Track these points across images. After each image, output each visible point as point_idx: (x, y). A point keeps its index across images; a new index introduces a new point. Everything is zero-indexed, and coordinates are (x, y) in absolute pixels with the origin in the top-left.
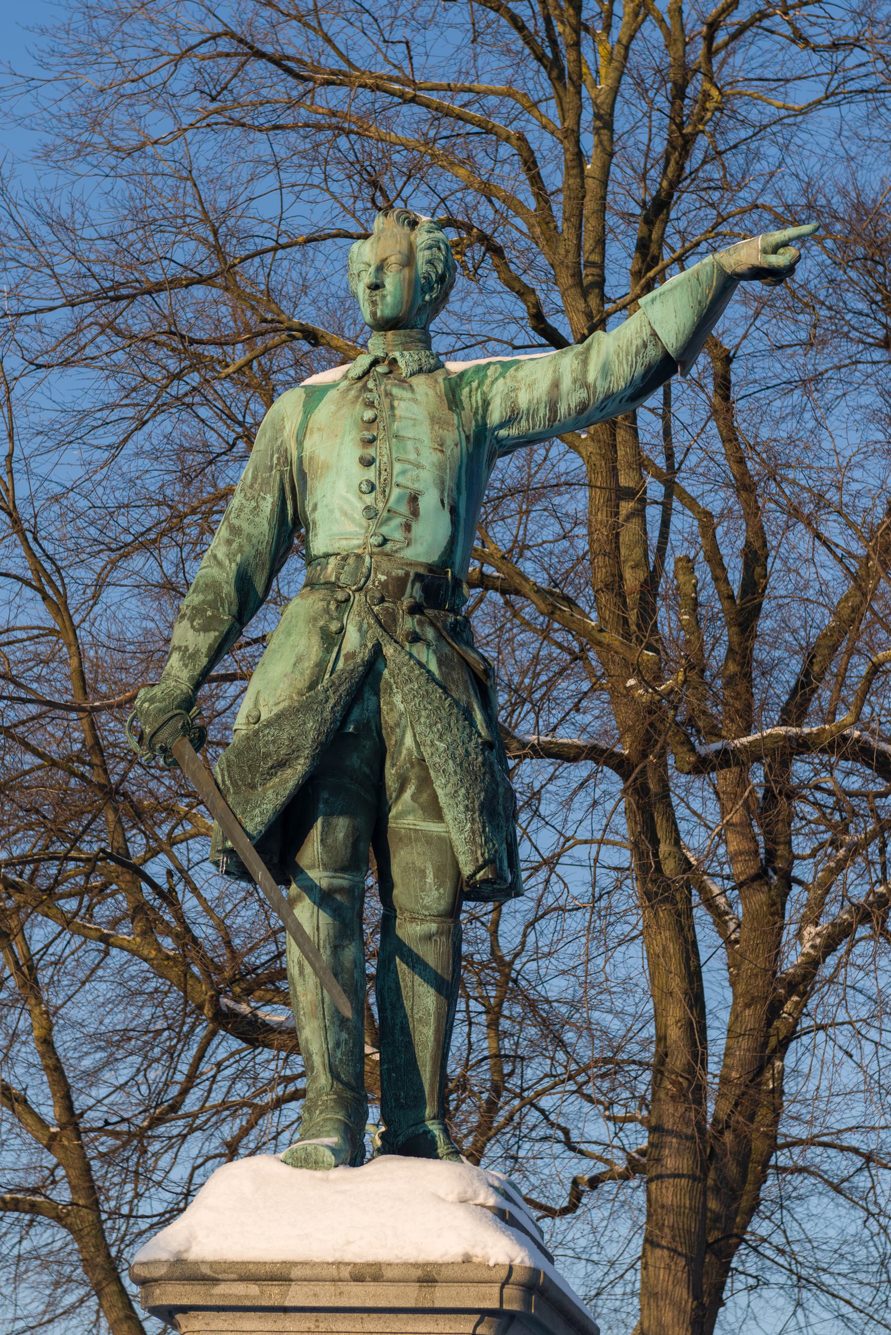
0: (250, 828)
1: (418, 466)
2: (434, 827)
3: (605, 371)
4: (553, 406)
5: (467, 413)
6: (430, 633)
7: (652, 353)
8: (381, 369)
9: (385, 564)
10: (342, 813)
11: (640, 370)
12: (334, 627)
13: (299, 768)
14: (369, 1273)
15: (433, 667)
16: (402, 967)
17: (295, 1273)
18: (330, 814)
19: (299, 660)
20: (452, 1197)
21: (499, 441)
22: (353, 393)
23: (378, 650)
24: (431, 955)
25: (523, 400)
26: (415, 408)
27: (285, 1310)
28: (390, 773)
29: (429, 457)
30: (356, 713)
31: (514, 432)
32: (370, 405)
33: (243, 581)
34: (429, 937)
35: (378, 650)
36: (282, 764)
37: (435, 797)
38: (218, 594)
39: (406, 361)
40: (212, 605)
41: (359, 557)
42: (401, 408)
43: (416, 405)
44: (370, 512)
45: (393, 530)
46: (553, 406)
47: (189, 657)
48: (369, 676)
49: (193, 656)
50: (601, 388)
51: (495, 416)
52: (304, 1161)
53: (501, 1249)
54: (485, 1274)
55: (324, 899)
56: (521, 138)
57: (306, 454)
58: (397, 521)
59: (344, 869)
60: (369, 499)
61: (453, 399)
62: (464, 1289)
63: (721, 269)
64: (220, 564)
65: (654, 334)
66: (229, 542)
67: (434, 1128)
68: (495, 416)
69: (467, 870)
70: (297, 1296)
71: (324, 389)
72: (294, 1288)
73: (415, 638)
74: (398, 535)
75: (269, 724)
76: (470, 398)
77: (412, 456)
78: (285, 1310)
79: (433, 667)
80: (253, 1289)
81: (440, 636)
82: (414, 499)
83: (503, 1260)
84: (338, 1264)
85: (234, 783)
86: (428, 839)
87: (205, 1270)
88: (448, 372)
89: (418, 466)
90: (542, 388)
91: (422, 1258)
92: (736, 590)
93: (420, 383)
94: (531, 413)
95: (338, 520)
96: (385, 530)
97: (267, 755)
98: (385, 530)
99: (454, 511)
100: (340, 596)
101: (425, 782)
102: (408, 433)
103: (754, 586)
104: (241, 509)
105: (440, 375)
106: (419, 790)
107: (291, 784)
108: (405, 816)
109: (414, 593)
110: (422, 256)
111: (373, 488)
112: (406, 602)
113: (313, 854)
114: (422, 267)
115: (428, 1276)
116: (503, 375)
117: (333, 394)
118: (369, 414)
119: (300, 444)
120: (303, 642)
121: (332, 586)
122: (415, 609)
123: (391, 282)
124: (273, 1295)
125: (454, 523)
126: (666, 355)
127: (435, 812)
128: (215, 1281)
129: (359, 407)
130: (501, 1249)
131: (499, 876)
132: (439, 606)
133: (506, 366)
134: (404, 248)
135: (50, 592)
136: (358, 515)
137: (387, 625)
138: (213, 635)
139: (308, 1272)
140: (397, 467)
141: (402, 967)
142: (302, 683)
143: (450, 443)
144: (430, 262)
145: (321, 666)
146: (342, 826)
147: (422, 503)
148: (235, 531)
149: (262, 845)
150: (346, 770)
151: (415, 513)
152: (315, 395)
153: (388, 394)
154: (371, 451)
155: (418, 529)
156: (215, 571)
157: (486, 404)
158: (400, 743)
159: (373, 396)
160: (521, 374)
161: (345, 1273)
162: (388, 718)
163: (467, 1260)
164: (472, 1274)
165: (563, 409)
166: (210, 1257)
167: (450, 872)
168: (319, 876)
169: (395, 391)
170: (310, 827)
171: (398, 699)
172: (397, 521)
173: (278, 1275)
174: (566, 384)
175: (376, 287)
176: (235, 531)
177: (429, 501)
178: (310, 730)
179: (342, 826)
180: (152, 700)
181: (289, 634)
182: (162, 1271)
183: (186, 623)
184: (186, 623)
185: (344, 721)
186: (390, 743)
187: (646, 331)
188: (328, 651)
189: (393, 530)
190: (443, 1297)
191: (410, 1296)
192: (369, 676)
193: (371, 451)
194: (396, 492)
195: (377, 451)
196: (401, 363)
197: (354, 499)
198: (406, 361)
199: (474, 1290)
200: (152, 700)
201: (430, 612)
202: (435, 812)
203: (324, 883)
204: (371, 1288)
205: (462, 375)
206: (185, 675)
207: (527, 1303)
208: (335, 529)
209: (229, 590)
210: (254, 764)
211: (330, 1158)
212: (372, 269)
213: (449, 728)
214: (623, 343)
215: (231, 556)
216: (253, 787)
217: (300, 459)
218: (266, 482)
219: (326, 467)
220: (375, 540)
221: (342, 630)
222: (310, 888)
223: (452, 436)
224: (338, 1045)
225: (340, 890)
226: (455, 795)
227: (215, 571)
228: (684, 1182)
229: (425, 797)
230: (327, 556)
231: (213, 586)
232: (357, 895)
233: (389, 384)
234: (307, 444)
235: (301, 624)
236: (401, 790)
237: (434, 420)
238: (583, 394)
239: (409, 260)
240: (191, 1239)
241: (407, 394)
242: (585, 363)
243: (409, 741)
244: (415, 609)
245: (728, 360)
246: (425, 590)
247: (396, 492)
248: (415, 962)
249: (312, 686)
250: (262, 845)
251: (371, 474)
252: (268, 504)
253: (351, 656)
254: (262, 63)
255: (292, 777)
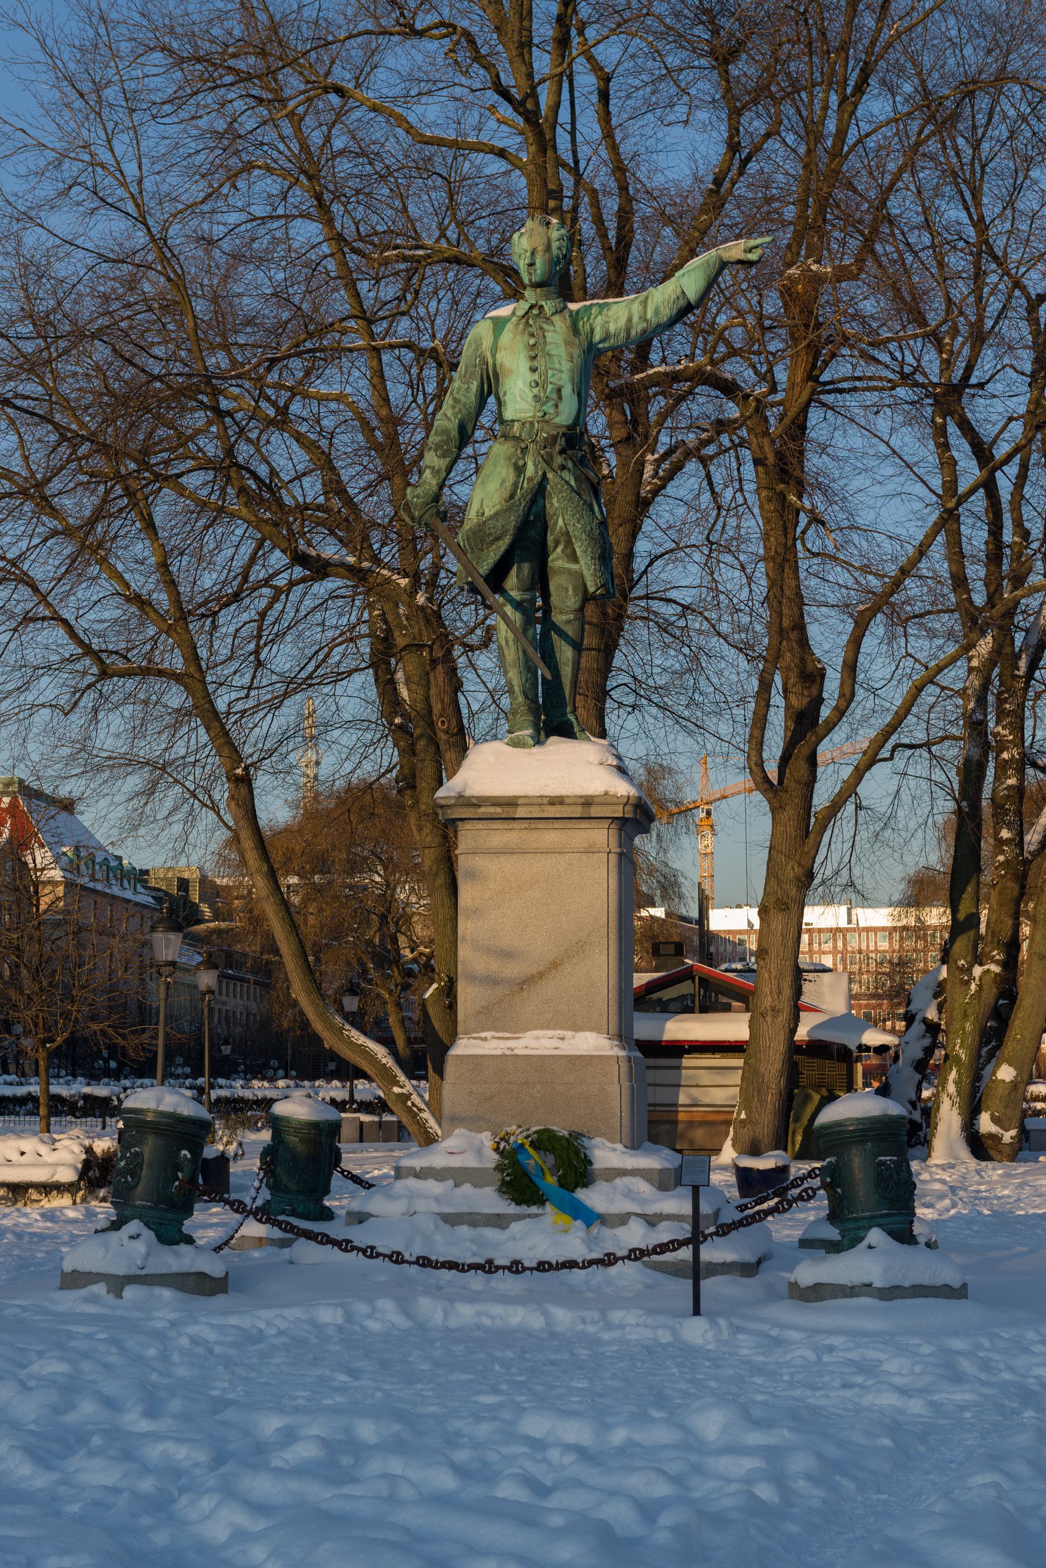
0: (481, 572)
1: (561, 371)
2: (574, 567)
3: (657, 312)
4: (628, 333)
5: (583, 337)
6: (570, 464)
7: (682, 302)
8: (535, 312)
9: (546, 428)
10: (526, 561)
11: (675, 311)
12: (521, 463)
13: (507, 540)
14: (557, 801)
15: (572, 483)
16: (555, 636)
17: (520, 801)
18: (520, 562)
19: (503, 481)
20: (596, 762)
21: (598, 350)
22: (521, 327)
23: (544, 475)
24: (570, 630)
25: (612, 328)
26: (556, 336)
27: (514, 819)
28: (550, 539)
29: (566, 366)
31: (607, 345)
32: (532, 335)
33: (462, 428)
34: (569, 622)
35: (544, 475)
36: (497, 539)
37: (574, 551)
38: (449, 436)
39: (548, 307)
40: (446, 442)
41: (532, 423)
42: (549, 336)
43: (557, 333)
45: (549, 408)
46: (628, 332)
47: (436, 472)
48: (540, 491)
49: (438, 471)
51: (597, 337)
52: (517, 744)
53: (622, 788)
54: (615, 801)
55: (518, 606)
57: (498, 362)
59: (527, 590)
60: (536, 391)
61: (575, 330)
62: (605, 808)
63: (721, 259)
64: (448, 419)
65: (683, 292)
66: (453, 407)
67: (571, 718)
68: (597, 337)
69: (591, 589)
70: (521, 812)
71: (505, 320)
72: (520, 809)
73: (563, 468)
74: (552, 411)
75: (491, 518)
76: (583, 327)
77: (557, 366)
78: (514, 819)
79: (572, 483)
80: (499, 810)
81: (575, 465)
82: (559, 390)
83: (625, 793)
84: (542, 797)
85: (471, 548)
86: (570, 572)
87: (474, 801)
88: (571, 312)
89: (561, 371)
90: (623, 321)
91: (584, 793)
92: (613, 241)
93: (556, 319)
94: (616, 336)
95: (519, 398)
96: (545, 408)
97: (490, 534)
98: (545, 408)
99: (579, 395)
100: (523, 445)
101: (569, 543)
102: (554, 352)
103: (625, 241)
104: (459, 389)
105: (566, 313)
106: (566, 547)
107: (503, 549)
108: (557, 559)
109: (561, 442)
110: (555, 245)
111: (537, 384)
112: (558, 448)
113: (512, 582)
115: (587, 802)
116: (600, 313)
117: (509, 326)
118: (532, 341)
119: (494, 356)
120: (504, 471)
121: (518, 439)
122: (562, 452)
123: (539, 261)
124: (509, 812)
125: (580, 401)
126: (689, 303)
127: (574, 558)
128: (479, 806)
129: (526, 336)
130: (622, 788)
131: (608, 592)
132: (573, 448)
133: (601, 307)
134: (545, 240)
135: (172, 276)
136: (530, 399)
137: (548, 461)
138: (448, 459)
139: (526, 801)
140: (550, 373)
141: (555, 636)
142: (506, 495)
143: (575, 356)
144: (559, 248)
145: (515, 485)
146: (526, 567)
148: (456, 401)
149: (487, 579)
150: (529, 538)
151: (560, 398)
152: (499, 324)
153: (541, 328)
154: (535, 363)
155: (562, 407)
156: (446, 423)
157: (592, 330)
158: (556, 523)
159: (533, 330)
160: (610, 313)
161: (546, 801)
162: (549, 511)
163: (606, 794)
164: (609, 800)
165: (633, 333)
166: (476, 794)
167: (581, 589)
168: (515, 594)
169: (545, 326)
170: (510, 569)
171: (555, 501)
173: (512, 802)
174: (635, 319)
175: (532, 265)
176: (456, 401)
177: (567, 391)
178: (513, 520)
179: (526, 567)
180: (418, 497)
181: (495, 466)
182: (453, 802)
183: (432, 452)
184: (432, 452)
186: (551, 523)
187: (679, 291)
188: (519, 476)
190: (595, 811)
191: (578, 811)
192: (540, 491)
193: (535, 363)
194: (550, 387)
195: (540, 363)
196: (546, 308)
197: (527, 391)
198: (548, 307)
199: (610, 808)
200: (418, 497)
201: (569, 452)
202: (574, 558)
203: (518, 598)
204: (558, 808)
205: (578, 312)
206: (434, 482)
207: (635, 813)
208: (518, 406)
209: (454, 434)
210: (481, 536)
211: (530, 741)
212: (528, 254)
213: (582, 516)
214: (666, 296)
215: (455, 415)
216: (482, 550)
217: (494, 365)
218: (473, 374)
219: (510, 371)
220: (540, 414)
221: (525, 464)
222: (510, 600)
223: (576, 352)
225: (526, 601)
226: (585, 551)
227: (446, 423)
228: (593, 653)
229: (568, 551)
230: (513, 421)
231: (445, 432)
232: (532, 601)
233: (540, 322)
234: (498, 356)
235: (502, 460)
236: (556, 547)
237: (567, 343)
239: (548, 248)
240: (466, 785)
241: (551, 328)
242: (645, 307)
243: (560, 522)
244: (562, 452)
245: (607, 79)
246: (567, 441)
247: (550, 387)
248: (562, 634)
249: (512, 496)
250: (487, 579)
251: (536, 376)
252: (474, 386)
253: (530, 479)
255: (503, 545)
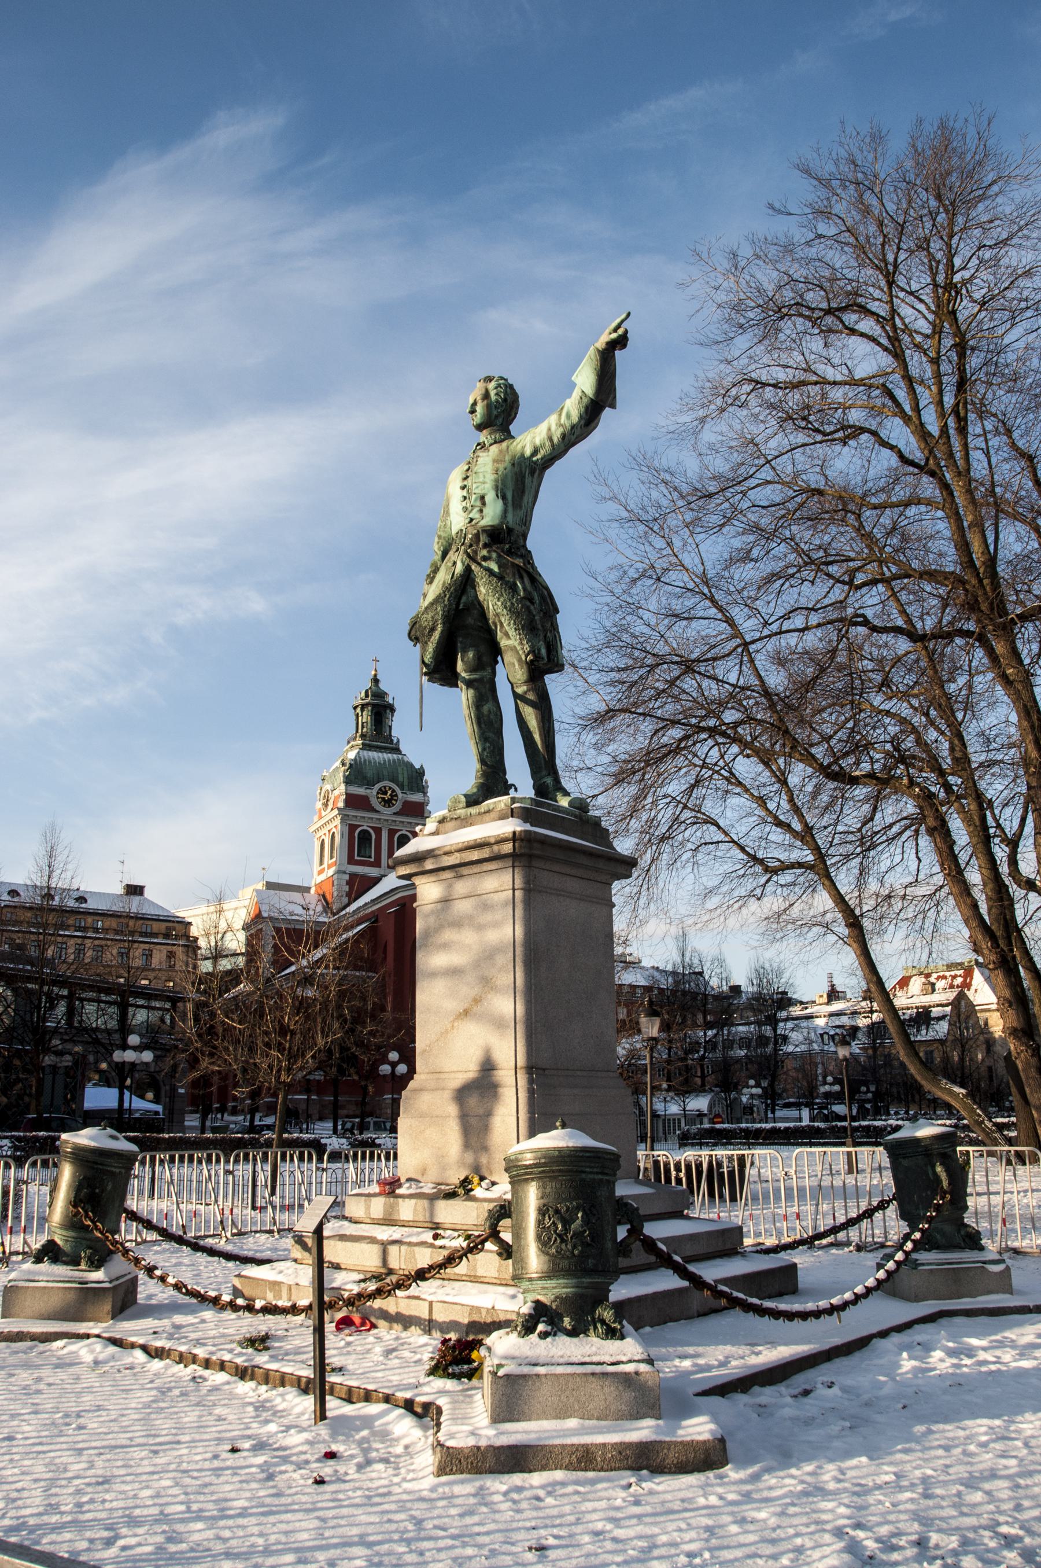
3: (568, 416)
4: (551, 439)
7: (585, 400)
23: (468, 570)
30: (464, 599)
36: (433, 629)
44: (465, 509)
45: (475, 514)
46: (551, 439)
50: (568, 425)
56: (884, 385)
58: (476, 510)
73: (485, 558)
82: (482, 498)
94: (543, 446)
109: (483, 539)
110: (492, 393)
114: (493, 397)
122: (485, 546)
125: (505, 504)
137: (472, 558)
147: (487, 499)
151: (484, 504)
162: (481, 598)
165: (555, 440)
172: (476, 510)
185: (458, 604)
189: (475, 514)
195: (468, 482)
224: (484, 749)
238: (561, 430)
239: (486, 396)
244: (485, 546)
254: (768, 389)
